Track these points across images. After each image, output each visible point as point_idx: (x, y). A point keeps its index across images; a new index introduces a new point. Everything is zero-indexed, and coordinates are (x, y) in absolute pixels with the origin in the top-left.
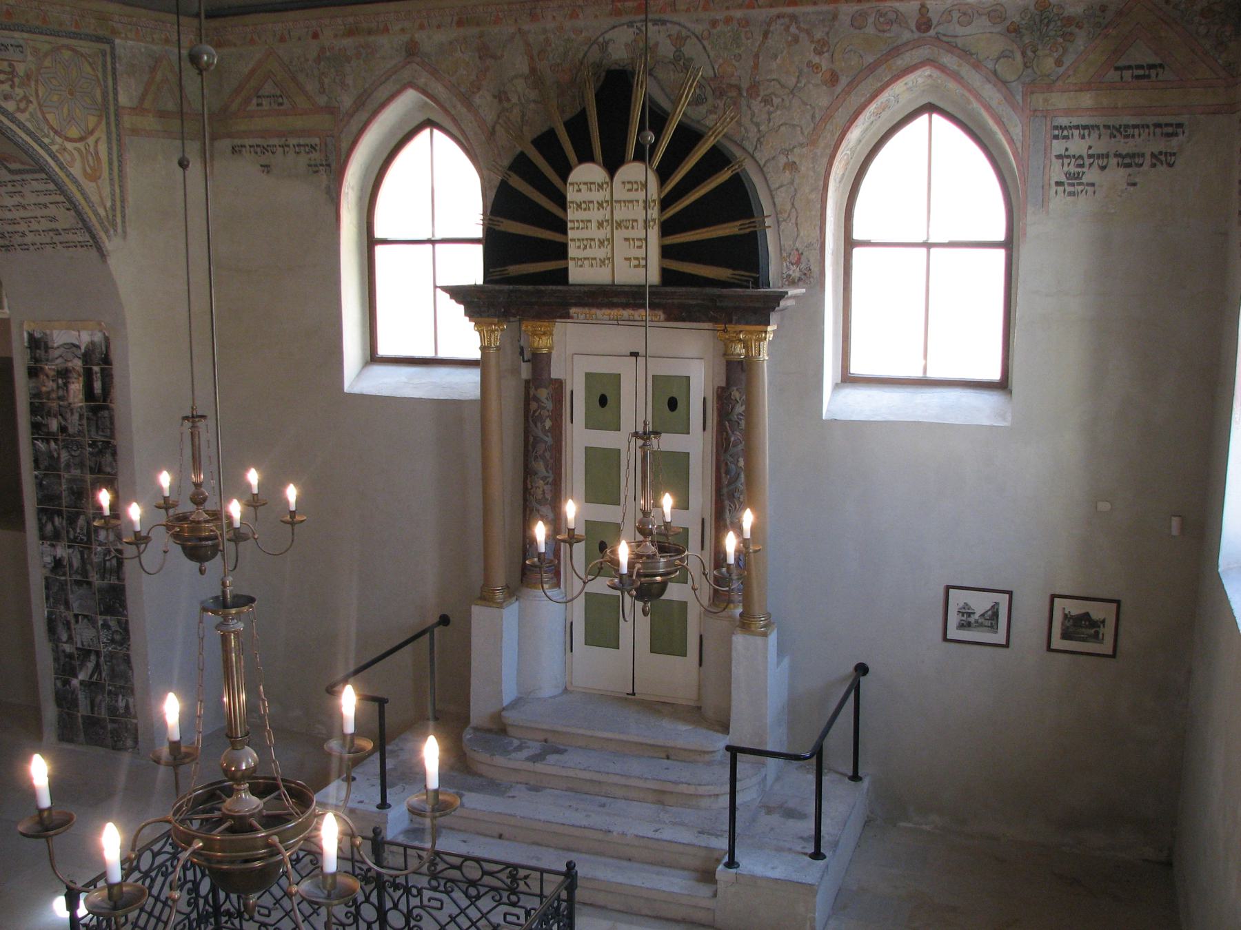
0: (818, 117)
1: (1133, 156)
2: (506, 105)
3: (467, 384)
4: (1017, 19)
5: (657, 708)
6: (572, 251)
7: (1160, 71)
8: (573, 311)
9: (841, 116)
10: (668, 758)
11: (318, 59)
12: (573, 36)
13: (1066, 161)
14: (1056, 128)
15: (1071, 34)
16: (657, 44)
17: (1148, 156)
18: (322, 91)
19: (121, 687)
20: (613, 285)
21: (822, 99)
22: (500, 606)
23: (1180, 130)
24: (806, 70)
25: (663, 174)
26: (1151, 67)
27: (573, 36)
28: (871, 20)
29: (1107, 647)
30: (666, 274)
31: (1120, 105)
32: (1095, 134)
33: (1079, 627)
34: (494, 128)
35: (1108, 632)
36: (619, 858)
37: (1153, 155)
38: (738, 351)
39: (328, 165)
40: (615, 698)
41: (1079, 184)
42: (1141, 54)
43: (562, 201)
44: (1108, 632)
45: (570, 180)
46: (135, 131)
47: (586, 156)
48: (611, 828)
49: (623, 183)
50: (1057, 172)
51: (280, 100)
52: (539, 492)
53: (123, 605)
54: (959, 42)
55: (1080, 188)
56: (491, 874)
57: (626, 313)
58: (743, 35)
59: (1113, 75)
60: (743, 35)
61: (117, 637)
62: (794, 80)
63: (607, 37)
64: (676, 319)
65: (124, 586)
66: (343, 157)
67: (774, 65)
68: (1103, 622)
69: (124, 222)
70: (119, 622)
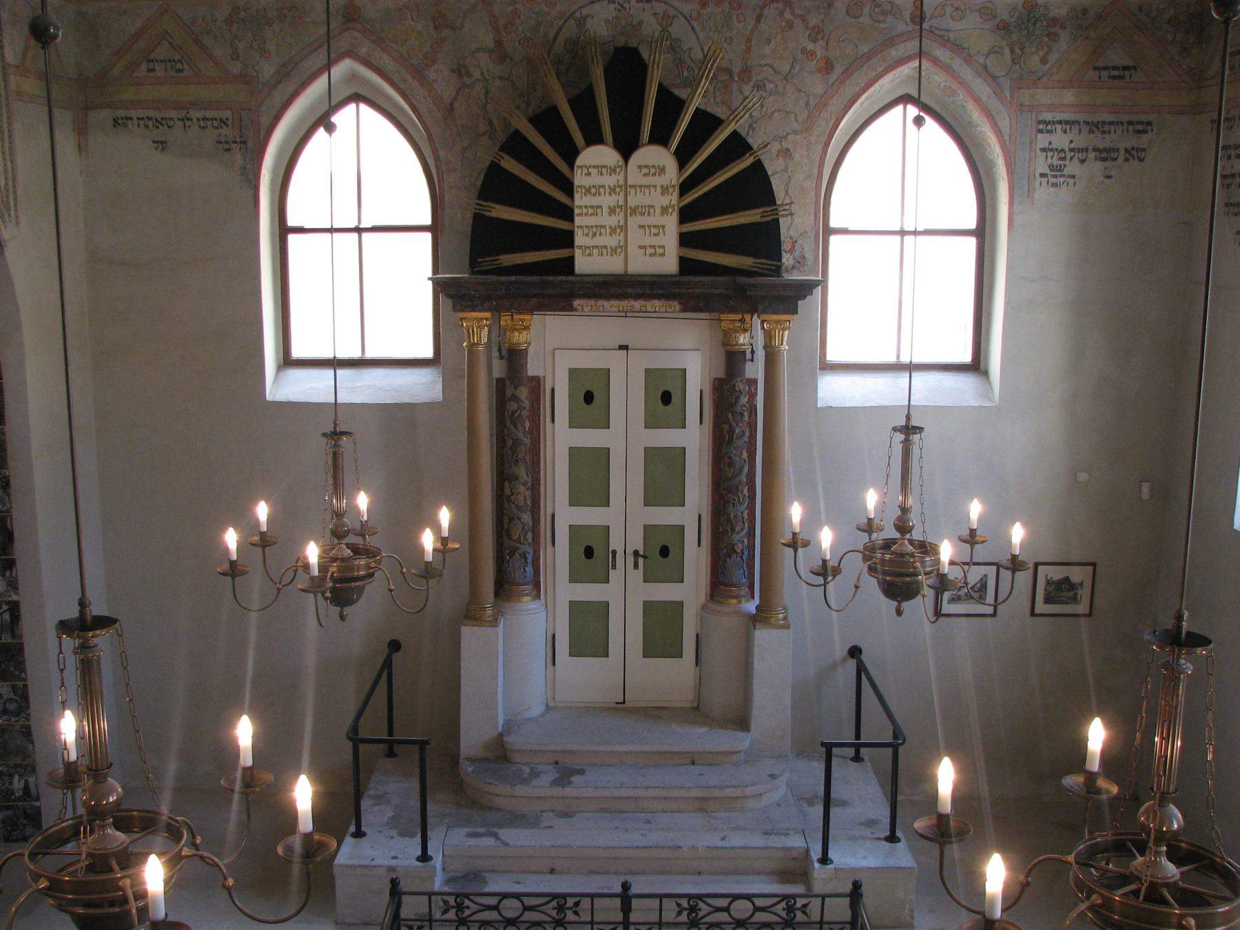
0: (812, 102)
1: (1108, 150)
2: (467, 80)
3: (421, 387)
4: (1006, 17)
5: (656, 713)
6: (579, 240)
7: (1133, 72)
8: (576, 303)
9: (835, 103)
10: (693, 763)
11: (229, 21)
12: (546, 9)
13: (1050, 154)
14: (1040, 122)
15: (1055, 34)
16: (640, 23)
17: (1122, 151)
18: (236, 57)
19: (16, 766)
20: (626, 275)
21: (816, 85)
22: (494, 623)
23: (1149, 128)
24: (800, 56)
25: (683, 156)
26: (1126, 68)
27: (546, 9)
28: (866, 10)
29: (1082, 608)
30: (683, 261)
31: (1098, 102)
32: (1075, 129)
33: (1061, 591)
34: (452, 104)
35: (1084, 593)
36: (686, 873)
37: (1126, 150)
38: (741, 341)
39: (244, 142)
40: (605, 708)
41: (1061, 176)
42: (1117, 56)
43: (568, 187)
44: (1084, 593)
45: (579, 162)
46: (20, 95)
47: (594, 138)
48: (681, 843)
49: (639, 167)
50: (1041, 165)
51: (179, 66)
52: (521, 498)
53: (21, 666)
54: (952, 36)
55: (1062, 180)
56: (763, 909)
57: (637, 304)
58: (734, 18)
59: (1092, 75)
60: (734, 18)
61: (12, 707)
62: (788, 67)
63: (585, 11)
64: (694, 310)
65: (22, 644)
66: (263, 133)
67: (767, 50)
68: (1081, 584)
69: (16, 205)
70: (14, 689)
